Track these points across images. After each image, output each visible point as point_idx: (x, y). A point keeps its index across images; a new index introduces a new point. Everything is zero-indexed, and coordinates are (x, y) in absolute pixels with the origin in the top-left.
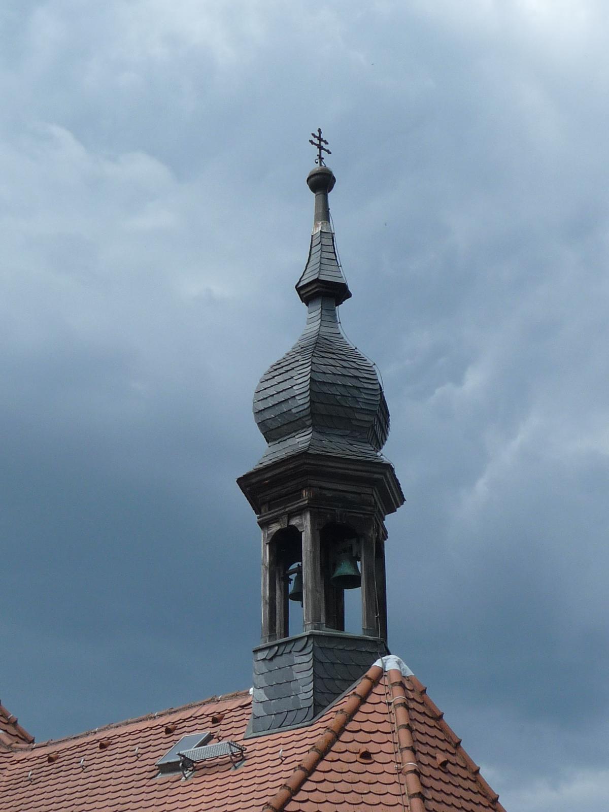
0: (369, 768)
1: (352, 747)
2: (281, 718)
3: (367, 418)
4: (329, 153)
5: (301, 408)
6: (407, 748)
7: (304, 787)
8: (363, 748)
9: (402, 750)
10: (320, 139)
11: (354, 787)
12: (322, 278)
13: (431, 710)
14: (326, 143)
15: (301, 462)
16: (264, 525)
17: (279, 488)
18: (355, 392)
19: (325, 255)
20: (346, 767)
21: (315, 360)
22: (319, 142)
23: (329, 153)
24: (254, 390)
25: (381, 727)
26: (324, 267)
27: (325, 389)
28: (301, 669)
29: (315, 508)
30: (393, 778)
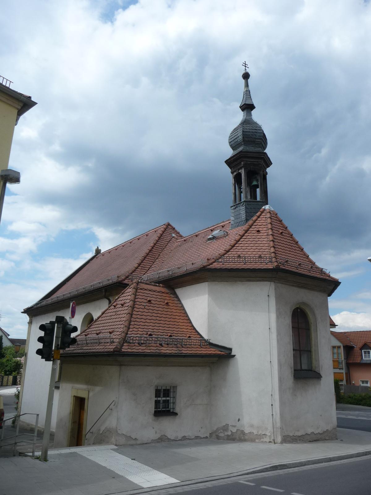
0: (259, 234)
1: (255, 229)
2: (238, 224)
3: (259, 140)
4: (248, 68)
5: (241, 139)
6: (270, 229)
7: (240, 240)
8: (258, 229)
9: (268, 229)
10: (245, 64)
11: (255, 240)
12: (246, 103)
13: (278, 219)
14: (247, 65)
15: (240, 154)
16: (232, 173)
17: (236, 162)
18: (256, 134)
19: (247, 97)
20: (253, 235)
21: (244, 126)
22: (245, 65)
23: (248, 68)
24: (229, 136)
25: (263, 224)
26: (247, 100)
27: (247, 133)
28: (242, 210)
29: (245, 167)
30: (265, 237)
